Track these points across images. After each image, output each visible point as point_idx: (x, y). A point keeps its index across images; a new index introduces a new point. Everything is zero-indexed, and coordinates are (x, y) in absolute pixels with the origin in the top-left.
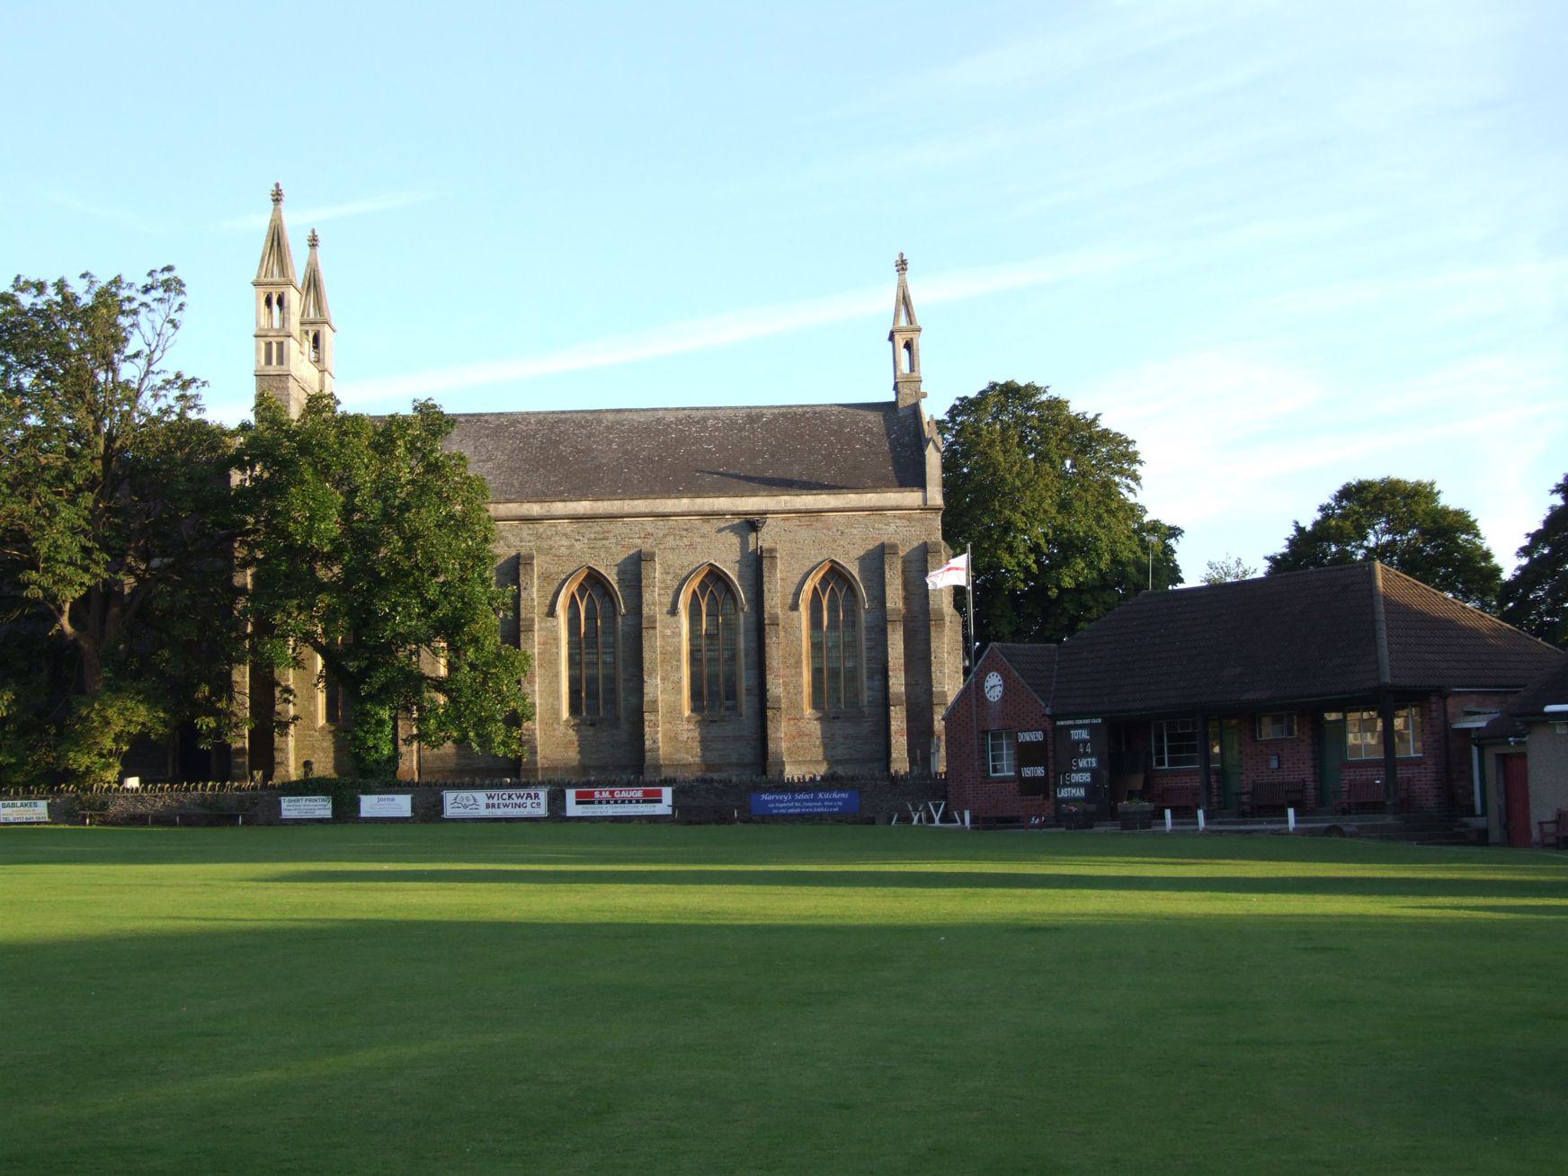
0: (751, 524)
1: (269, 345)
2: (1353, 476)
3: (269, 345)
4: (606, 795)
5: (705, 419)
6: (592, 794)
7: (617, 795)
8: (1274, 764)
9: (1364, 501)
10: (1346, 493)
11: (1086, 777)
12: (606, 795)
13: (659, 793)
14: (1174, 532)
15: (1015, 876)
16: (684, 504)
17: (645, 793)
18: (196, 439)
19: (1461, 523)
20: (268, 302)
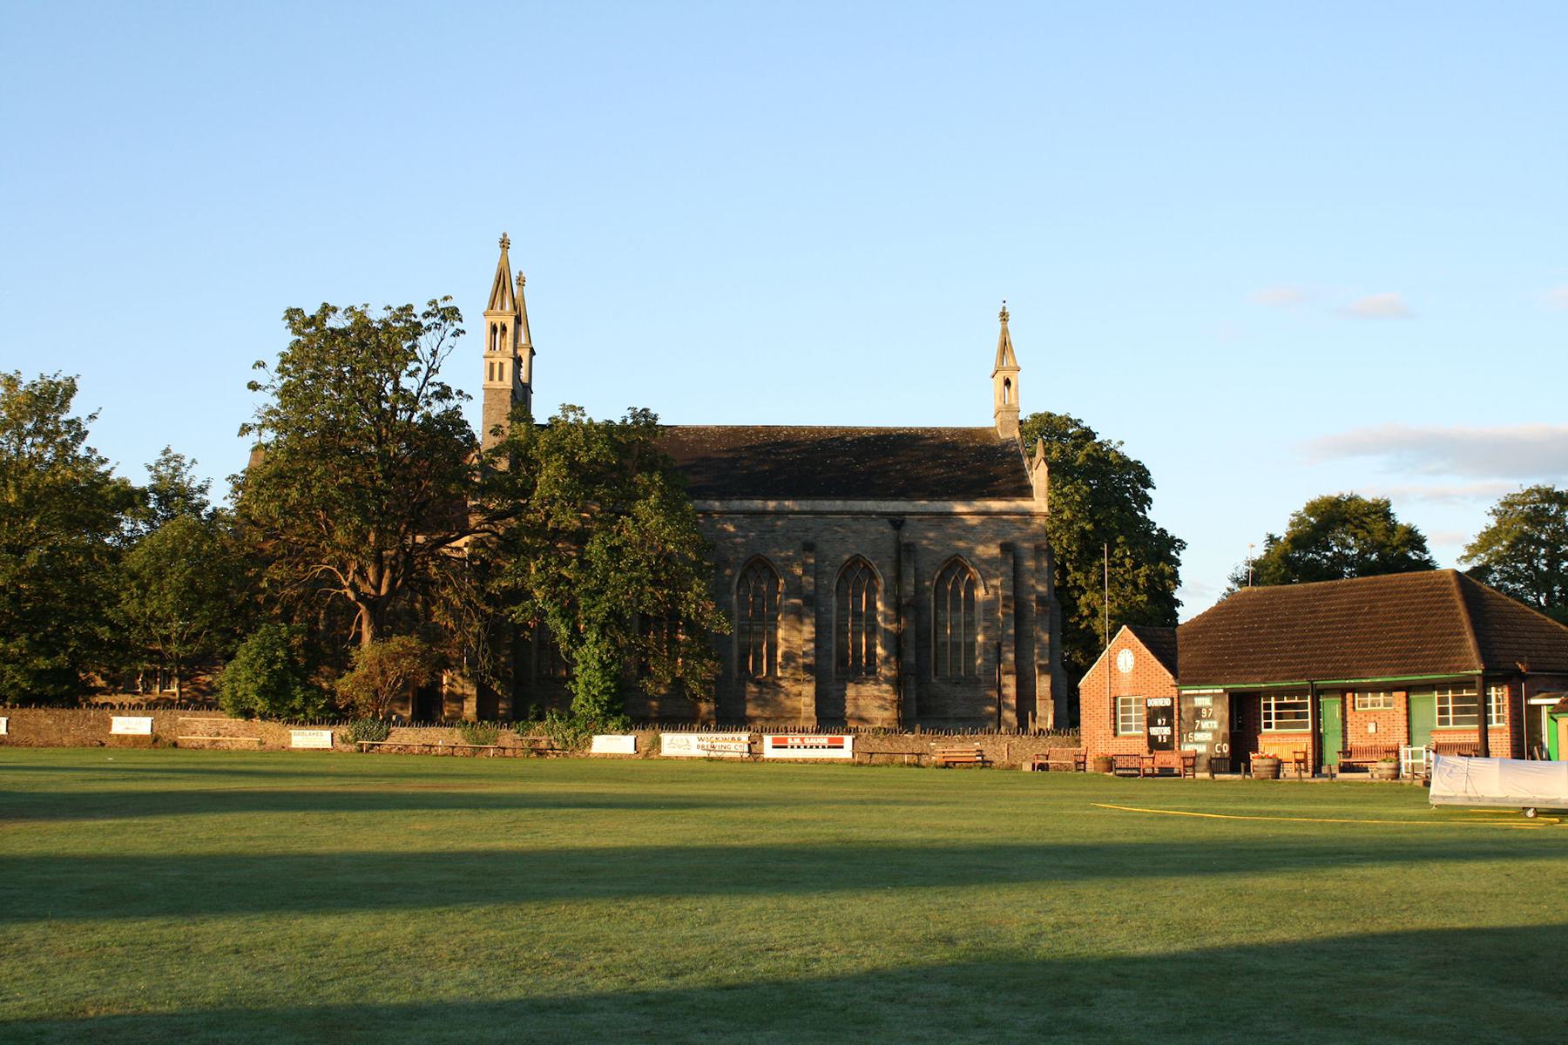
0: (897, 521)
1: (492, 365)
2: (1314, 496)
3: (492, 365)
4: (797, 741)
5: (843, 437)
6: (785, 740)
7: (807, 741)
8: (1372, 729)
9: (1332, 517)
10: (1313, 508)
11: (1208, 737)
12: (797, 741)
13: (842, 740)
14: (54, 395)
15: (304, 794)
16: (839, 504)
17: (830, 740)
18: (447, 433)
19: (1415, 540)
20: (494, 329)
